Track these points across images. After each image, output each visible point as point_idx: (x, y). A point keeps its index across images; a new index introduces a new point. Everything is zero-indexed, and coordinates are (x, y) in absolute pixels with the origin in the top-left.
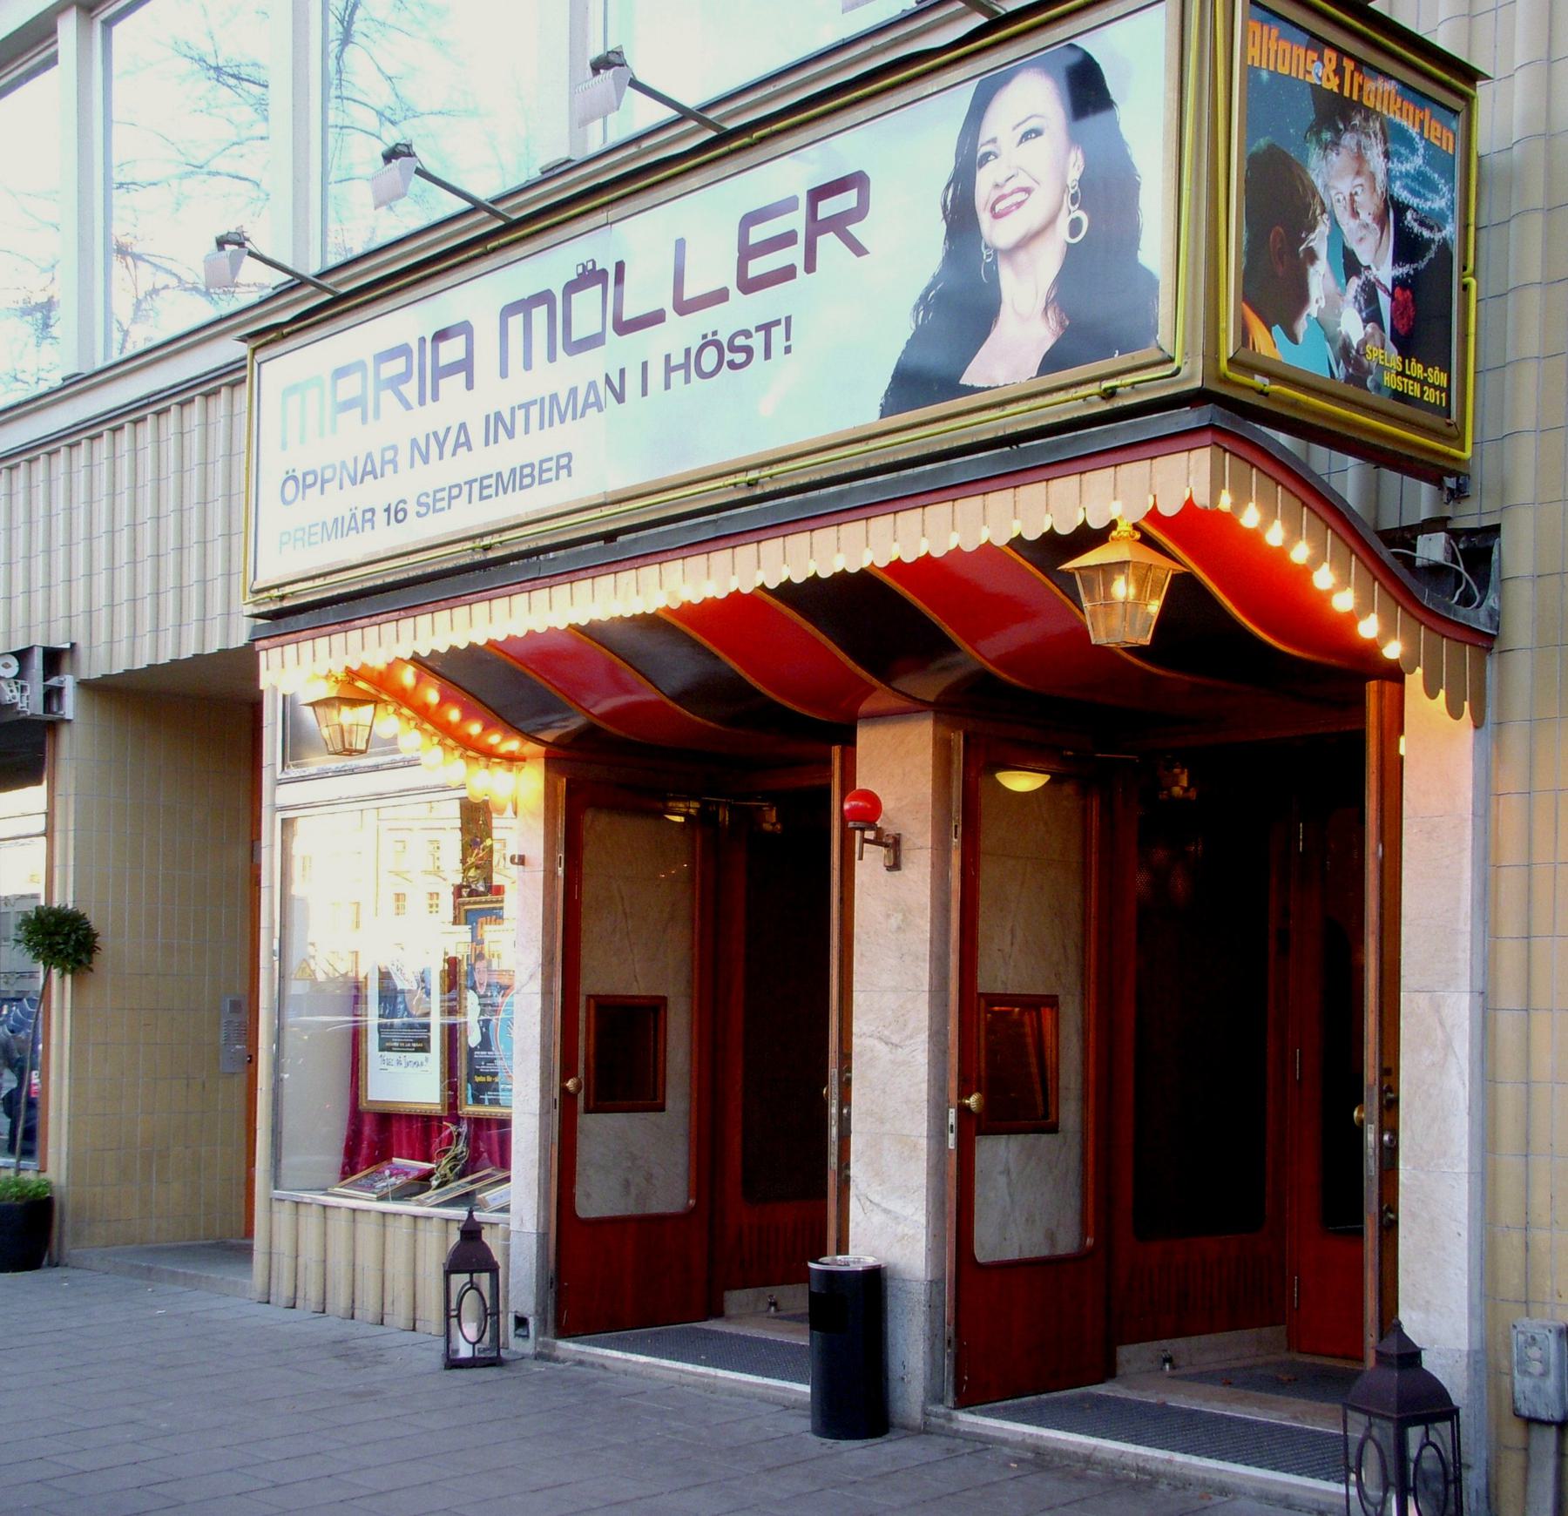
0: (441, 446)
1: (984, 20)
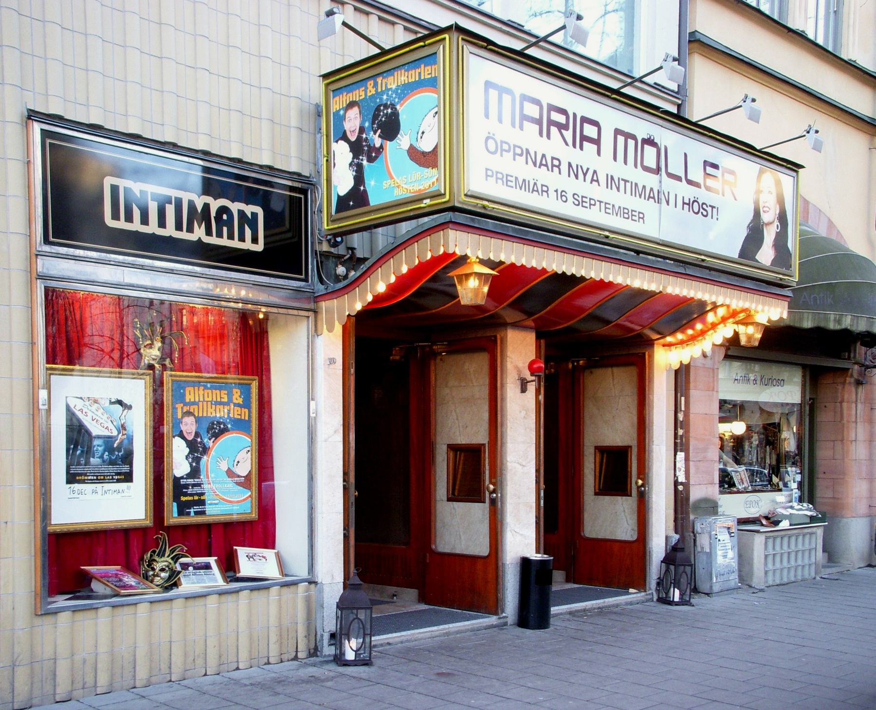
0: (585, 175)
1: (676, 112)
